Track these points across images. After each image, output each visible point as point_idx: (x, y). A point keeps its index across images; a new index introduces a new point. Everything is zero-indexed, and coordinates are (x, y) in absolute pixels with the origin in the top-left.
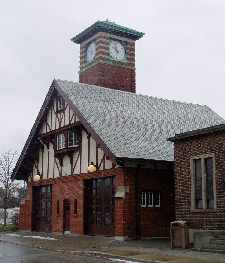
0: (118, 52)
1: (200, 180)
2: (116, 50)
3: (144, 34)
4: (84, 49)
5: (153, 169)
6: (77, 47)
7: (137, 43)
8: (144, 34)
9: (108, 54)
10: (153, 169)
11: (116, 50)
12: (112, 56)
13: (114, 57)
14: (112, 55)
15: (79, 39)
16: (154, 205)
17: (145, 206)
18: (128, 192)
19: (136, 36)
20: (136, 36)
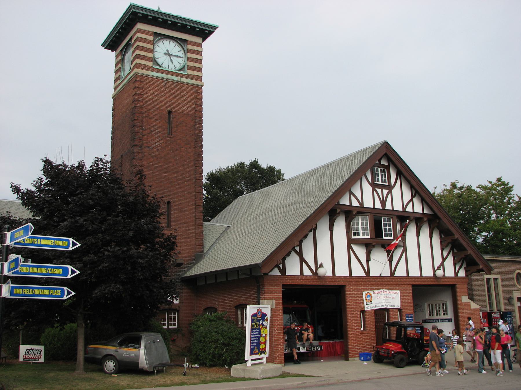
0: (168, 54)
1: (197, 210)
2: (170, 55)
3: (215, 28)
4: (120, 58)
5: (501, 351)
6: (111, 56)
7: (209, 46)
8: (215, 28)
9: (154, 60)
10: (501, 351)
11: (170, 55)
12: (160, 63)
13: (163, 65)
14: (160, 61)
15: (112, 43)
16: (168, 326)
17: (166, 327)
18: (274, 307)
19: (204, 31)
20: (204, 31)
